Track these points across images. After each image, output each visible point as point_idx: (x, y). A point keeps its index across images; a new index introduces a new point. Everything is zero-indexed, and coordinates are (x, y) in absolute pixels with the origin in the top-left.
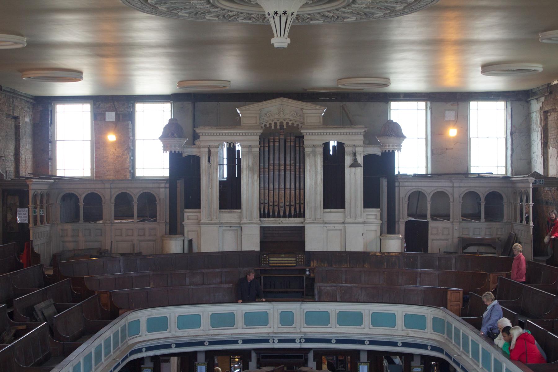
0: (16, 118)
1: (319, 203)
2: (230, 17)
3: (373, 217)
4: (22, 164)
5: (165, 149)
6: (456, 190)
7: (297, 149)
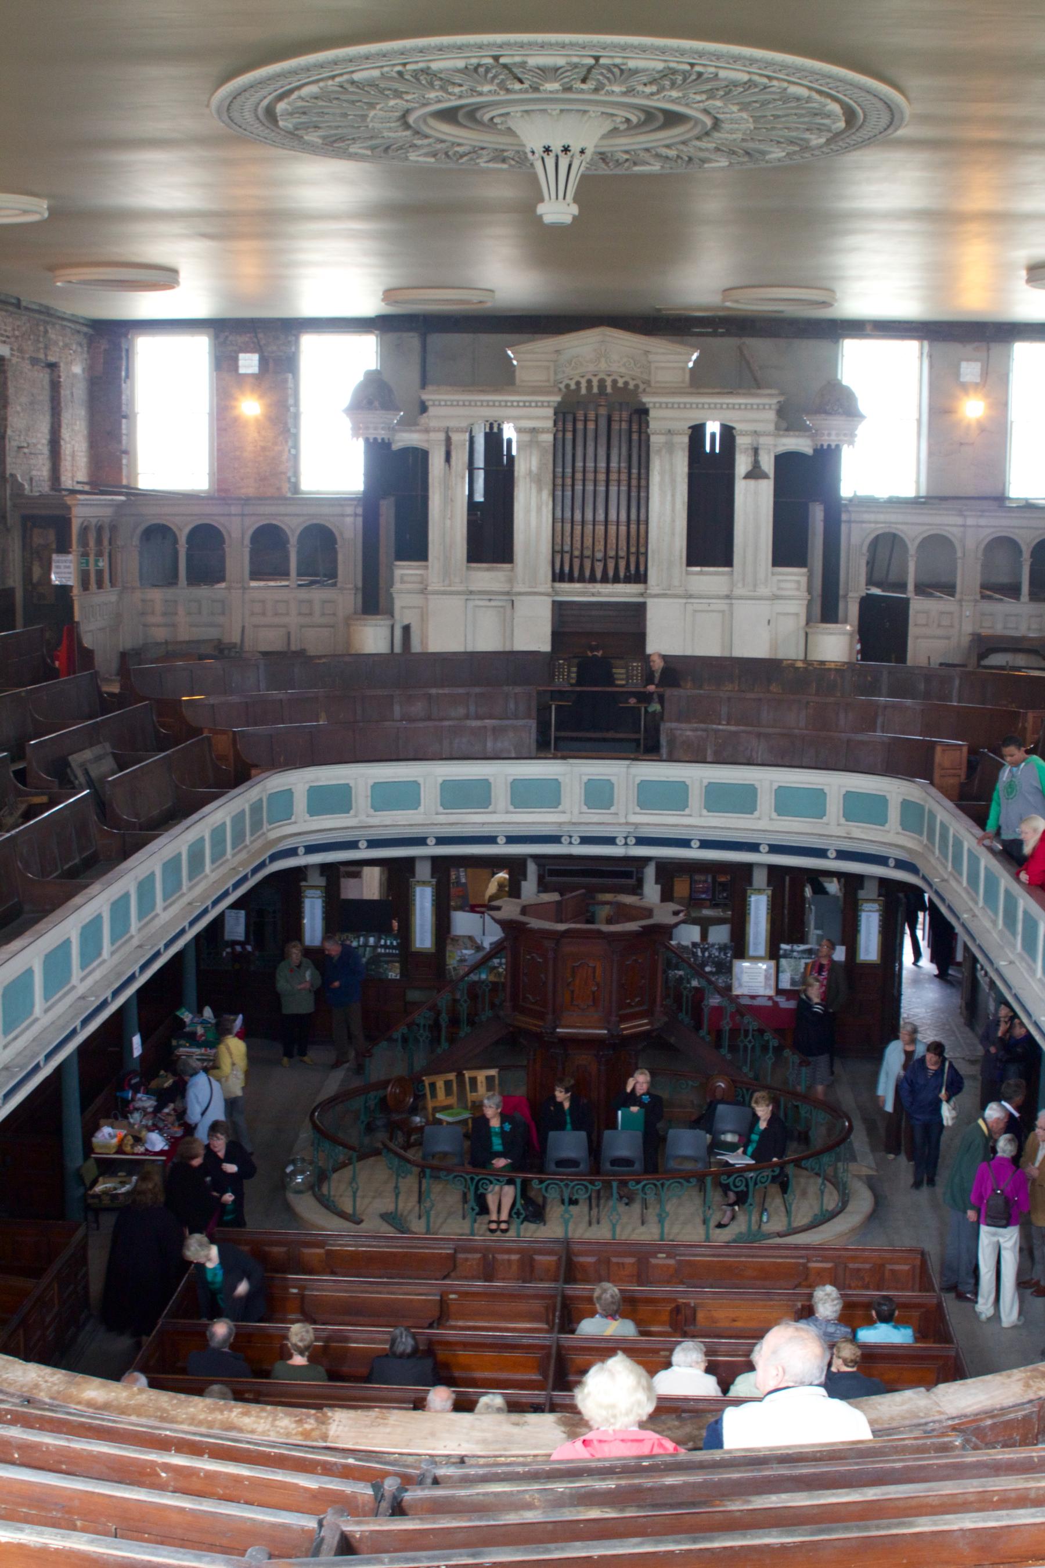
0: (53, 366)
1: (677, 553)
2: (462, 156)
3: (793, 585)
4: (66, 464)
5: (356, 431)
6: (970, 532)
7: (635, 437)
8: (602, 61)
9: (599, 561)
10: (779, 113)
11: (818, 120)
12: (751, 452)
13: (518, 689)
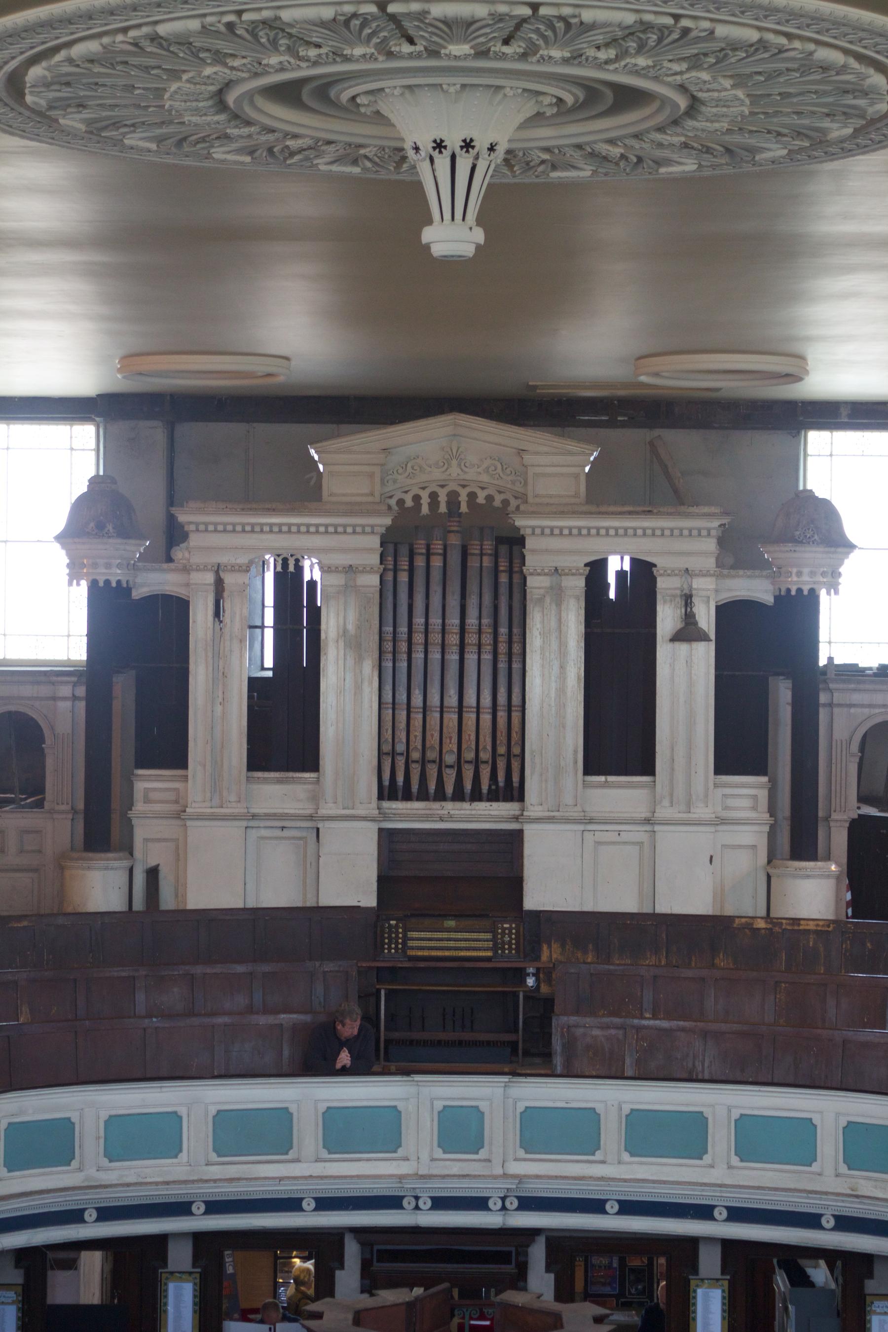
2: (292, 154)
3: (746, 803)
5: (75, 572)
7: (504, 579)
8: (543, 11)
9: (451, 767)
10: (791, 90)
11: (850, 100)
12: (680, 602)
13: (329, 966)
